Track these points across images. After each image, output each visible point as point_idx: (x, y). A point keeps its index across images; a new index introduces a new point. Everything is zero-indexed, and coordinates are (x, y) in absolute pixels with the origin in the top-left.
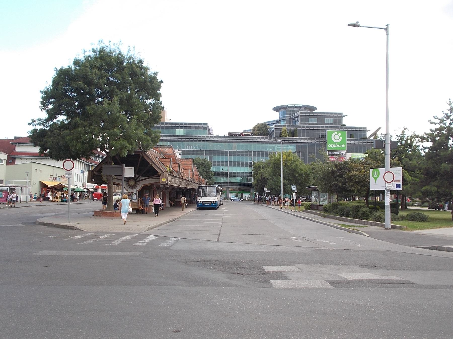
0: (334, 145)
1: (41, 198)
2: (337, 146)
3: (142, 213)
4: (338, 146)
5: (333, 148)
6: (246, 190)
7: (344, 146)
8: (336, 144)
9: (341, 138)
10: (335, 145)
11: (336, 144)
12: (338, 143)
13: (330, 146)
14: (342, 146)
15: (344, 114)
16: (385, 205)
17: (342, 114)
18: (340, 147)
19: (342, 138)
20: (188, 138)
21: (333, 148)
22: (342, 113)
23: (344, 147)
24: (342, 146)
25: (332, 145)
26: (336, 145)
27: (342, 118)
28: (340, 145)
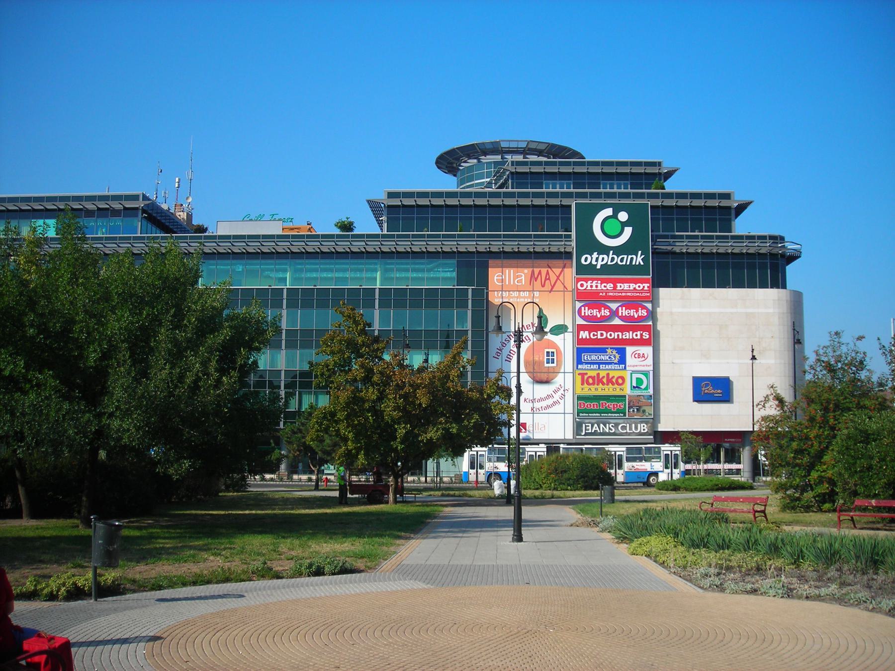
0: (601, 257)
4: (617, 260)
5: (598, 267)
8: (611, 252)
9: (628, 231)
10: (605, 256)
11: (611, 252)
12: (618, 250)
13: (586, 259)
14: (632, 259)
18: (624, 263)
19: (631, 228)
21: (598, 267)
24: (632, 259)
25: (595, 255)
26: (611, 256)
28: (626, 256)
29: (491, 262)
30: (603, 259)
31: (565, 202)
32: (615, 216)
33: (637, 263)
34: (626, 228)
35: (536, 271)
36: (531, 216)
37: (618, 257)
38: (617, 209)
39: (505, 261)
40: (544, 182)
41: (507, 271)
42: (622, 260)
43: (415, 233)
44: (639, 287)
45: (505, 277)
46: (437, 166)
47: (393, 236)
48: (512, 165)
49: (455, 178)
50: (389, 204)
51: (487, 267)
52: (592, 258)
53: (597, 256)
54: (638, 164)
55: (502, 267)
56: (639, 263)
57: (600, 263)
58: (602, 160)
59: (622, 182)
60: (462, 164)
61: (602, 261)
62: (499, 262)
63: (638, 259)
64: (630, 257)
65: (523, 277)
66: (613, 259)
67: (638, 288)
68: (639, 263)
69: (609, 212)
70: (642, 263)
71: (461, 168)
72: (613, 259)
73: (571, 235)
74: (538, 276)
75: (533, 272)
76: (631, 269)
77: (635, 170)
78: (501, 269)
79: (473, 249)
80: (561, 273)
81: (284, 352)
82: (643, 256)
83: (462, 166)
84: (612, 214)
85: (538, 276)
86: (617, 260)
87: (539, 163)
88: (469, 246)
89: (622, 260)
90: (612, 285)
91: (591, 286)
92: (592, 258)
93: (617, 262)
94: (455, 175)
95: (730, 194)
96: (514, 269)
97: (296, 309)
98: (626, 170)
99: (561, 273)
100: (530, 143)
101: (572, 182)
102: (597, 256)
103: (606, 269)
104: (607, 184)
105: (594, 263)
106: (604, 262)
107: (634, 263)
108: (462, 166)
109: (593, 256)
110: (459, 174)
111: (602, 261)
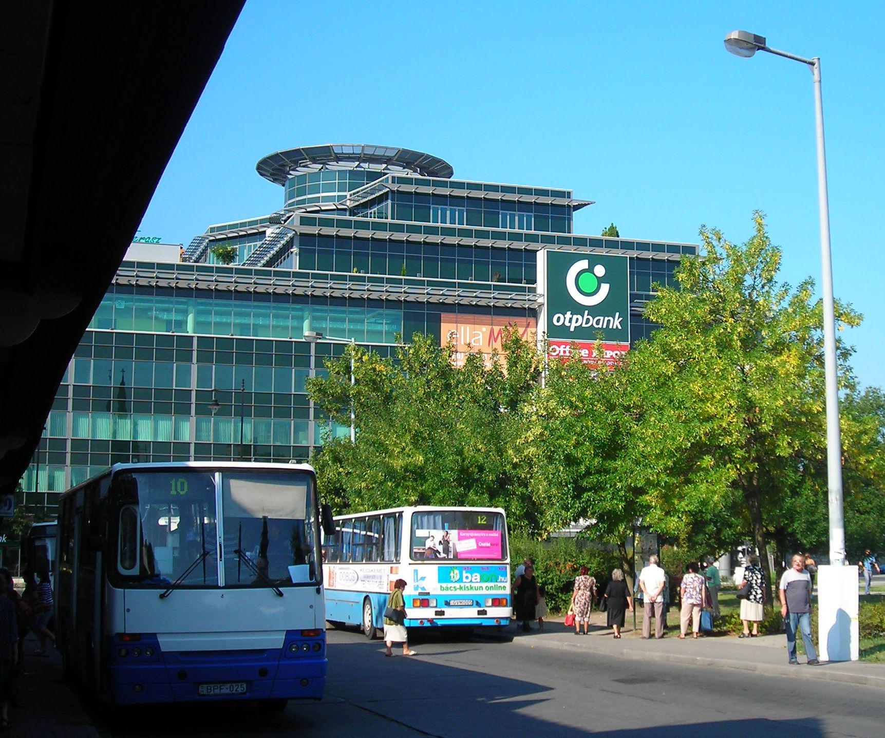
0: (575, 317)
1: (879, 624)
2: (587, 323)
3: (248, 575)
4: (593, 322)
5: (572, 329)
6: (625, 508)
7: (617, 322)
8: (586, 312)
9: (605, 288)
10: (580, 317)
11: (586, 312)
12: (594, 311)
13: (559, 319)
14: (609, 321)
15: (577, 198)
16: (40, 438)
17: (567, 195)
18: (600, 326)
19: (608, 285)
20: (187, 281)
21: (572, 329)
22: (569, 193)
23: (620, 327)
24: (609, 321)
25: (568, 315)
26: (586, 317)
27: (570, 214)
28: (602, 318)
29: (443, 315)
30: (577, 319)
31: (532, 246)
32: (590, 270)
33: (615, 327)
34: (602, 284)
35: (496, 329)
36: (474, 259)
37: (593, 319)
38: (594, 261)
39: (460, 316)
40: (432, 206)
41: (462, 328)
42: (598, 323)
43: (316, 272)
44: (616, 354)
45: (460, 335)
46: (259, 172)
47: (306, 276)
48: (393, 182)
49: (284, 188)
50: (302, 232)
51: (439, 322)
52: (565, 318)
53: (571, 316)
54: (494, 188)
55: (456, 322)
56: (617, 326)
57: (574, 325)
58: (503, 184)
59: (440, 207)
60: (291, 172)
61: (577, 322)
62: (452, 316)
63: (616, 323)
64: (607, 319)
65: (481, 337)
66: (588, 320)
67: (614, 356)
68: (617, 326)
69: (583, 264)
70: (620, 328)
71: (290, 177)
72: (588, 320)
73: (535, 288)
74: (498, 336)
75: (492, 331)
76: (609, 334)
77: (475, 194)
78: (455, 325)
79: (424, 299)
80: (524, 333)
81: (193, 419)
82: (621, 319)
83: (291, 175)
84: (587, 268)
85: (498, 336)
86: (593, 322)
87: (408, 181)
88: (423, 294)
89: (598, 323)
90: (587, 352)
91: (565, 352)
92: (565, 318)
93: (592, 325)
94: (284, 185)
95: (695, 248)
96: (470, 325)
97: (209, 364)
98: (532, 199)
99: (524, 333)
100: (365, 148)
101: (465, 209)
102: (571, 316)
103: (581, 332)
104: (455, 210)
105: (567, 324)
106: (579, 324)
107: (611, 327)
108: (291, 175)
109: (566, 316)
110: (287, 183)
111: (577, 322)
